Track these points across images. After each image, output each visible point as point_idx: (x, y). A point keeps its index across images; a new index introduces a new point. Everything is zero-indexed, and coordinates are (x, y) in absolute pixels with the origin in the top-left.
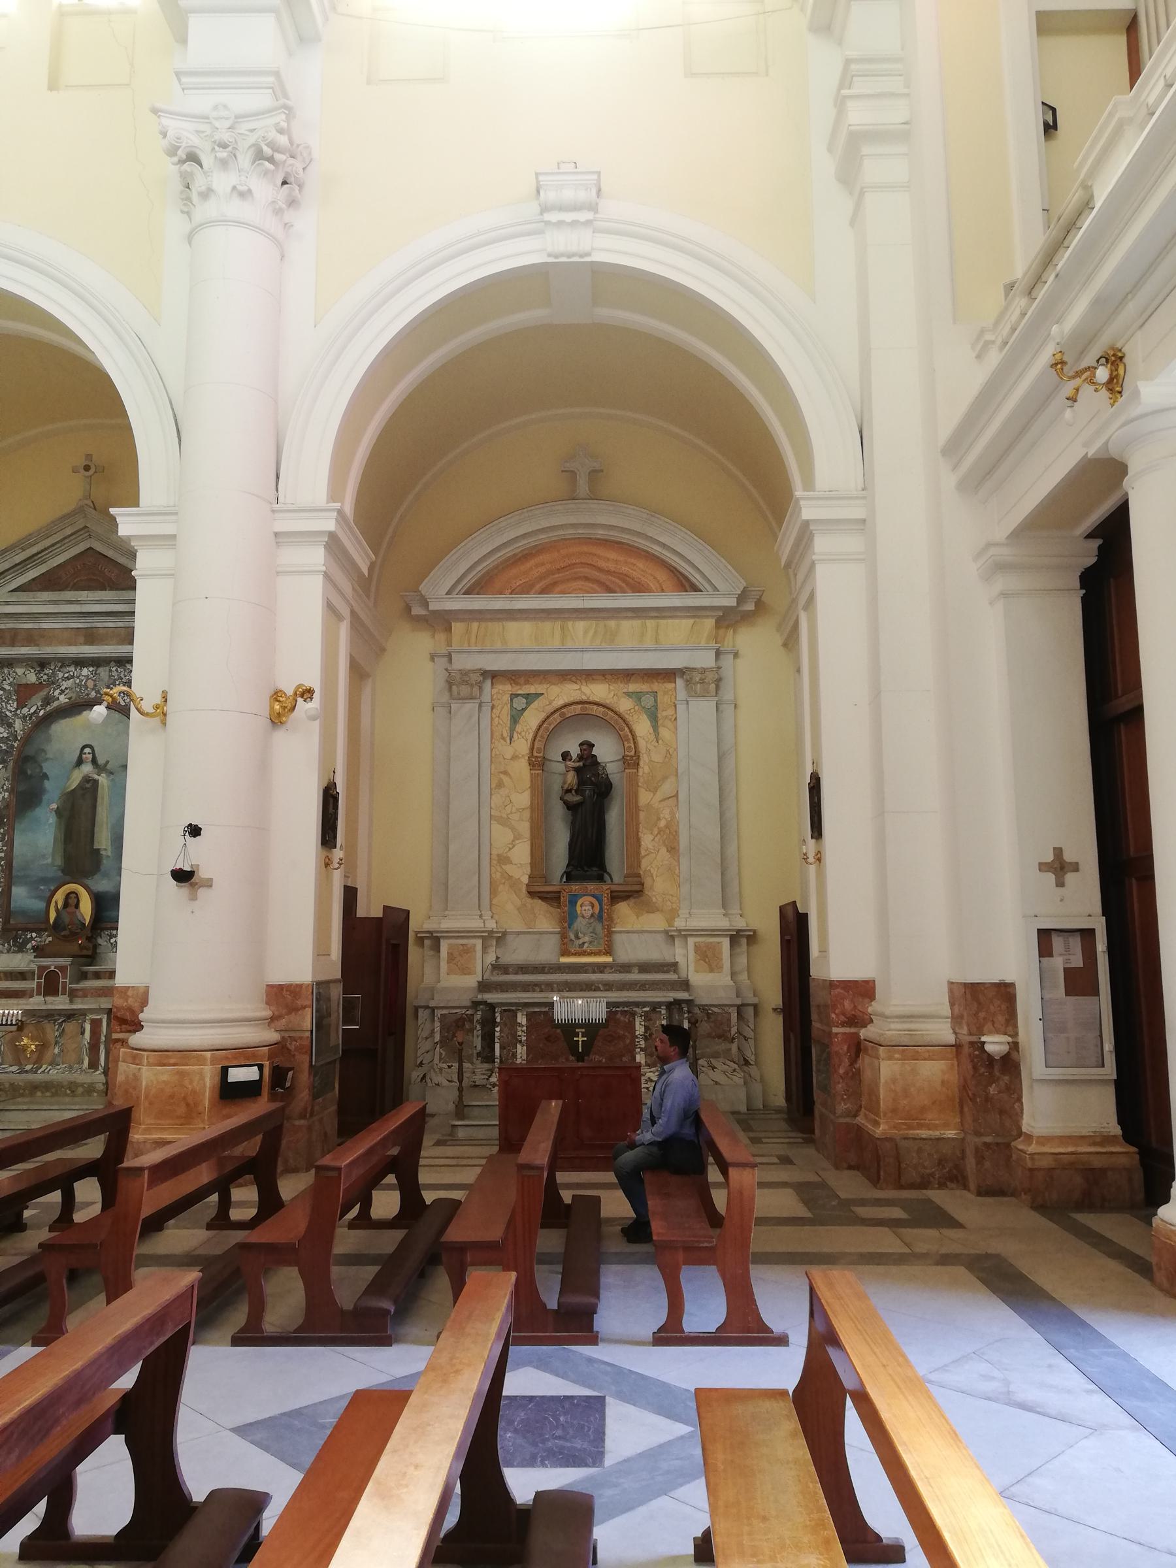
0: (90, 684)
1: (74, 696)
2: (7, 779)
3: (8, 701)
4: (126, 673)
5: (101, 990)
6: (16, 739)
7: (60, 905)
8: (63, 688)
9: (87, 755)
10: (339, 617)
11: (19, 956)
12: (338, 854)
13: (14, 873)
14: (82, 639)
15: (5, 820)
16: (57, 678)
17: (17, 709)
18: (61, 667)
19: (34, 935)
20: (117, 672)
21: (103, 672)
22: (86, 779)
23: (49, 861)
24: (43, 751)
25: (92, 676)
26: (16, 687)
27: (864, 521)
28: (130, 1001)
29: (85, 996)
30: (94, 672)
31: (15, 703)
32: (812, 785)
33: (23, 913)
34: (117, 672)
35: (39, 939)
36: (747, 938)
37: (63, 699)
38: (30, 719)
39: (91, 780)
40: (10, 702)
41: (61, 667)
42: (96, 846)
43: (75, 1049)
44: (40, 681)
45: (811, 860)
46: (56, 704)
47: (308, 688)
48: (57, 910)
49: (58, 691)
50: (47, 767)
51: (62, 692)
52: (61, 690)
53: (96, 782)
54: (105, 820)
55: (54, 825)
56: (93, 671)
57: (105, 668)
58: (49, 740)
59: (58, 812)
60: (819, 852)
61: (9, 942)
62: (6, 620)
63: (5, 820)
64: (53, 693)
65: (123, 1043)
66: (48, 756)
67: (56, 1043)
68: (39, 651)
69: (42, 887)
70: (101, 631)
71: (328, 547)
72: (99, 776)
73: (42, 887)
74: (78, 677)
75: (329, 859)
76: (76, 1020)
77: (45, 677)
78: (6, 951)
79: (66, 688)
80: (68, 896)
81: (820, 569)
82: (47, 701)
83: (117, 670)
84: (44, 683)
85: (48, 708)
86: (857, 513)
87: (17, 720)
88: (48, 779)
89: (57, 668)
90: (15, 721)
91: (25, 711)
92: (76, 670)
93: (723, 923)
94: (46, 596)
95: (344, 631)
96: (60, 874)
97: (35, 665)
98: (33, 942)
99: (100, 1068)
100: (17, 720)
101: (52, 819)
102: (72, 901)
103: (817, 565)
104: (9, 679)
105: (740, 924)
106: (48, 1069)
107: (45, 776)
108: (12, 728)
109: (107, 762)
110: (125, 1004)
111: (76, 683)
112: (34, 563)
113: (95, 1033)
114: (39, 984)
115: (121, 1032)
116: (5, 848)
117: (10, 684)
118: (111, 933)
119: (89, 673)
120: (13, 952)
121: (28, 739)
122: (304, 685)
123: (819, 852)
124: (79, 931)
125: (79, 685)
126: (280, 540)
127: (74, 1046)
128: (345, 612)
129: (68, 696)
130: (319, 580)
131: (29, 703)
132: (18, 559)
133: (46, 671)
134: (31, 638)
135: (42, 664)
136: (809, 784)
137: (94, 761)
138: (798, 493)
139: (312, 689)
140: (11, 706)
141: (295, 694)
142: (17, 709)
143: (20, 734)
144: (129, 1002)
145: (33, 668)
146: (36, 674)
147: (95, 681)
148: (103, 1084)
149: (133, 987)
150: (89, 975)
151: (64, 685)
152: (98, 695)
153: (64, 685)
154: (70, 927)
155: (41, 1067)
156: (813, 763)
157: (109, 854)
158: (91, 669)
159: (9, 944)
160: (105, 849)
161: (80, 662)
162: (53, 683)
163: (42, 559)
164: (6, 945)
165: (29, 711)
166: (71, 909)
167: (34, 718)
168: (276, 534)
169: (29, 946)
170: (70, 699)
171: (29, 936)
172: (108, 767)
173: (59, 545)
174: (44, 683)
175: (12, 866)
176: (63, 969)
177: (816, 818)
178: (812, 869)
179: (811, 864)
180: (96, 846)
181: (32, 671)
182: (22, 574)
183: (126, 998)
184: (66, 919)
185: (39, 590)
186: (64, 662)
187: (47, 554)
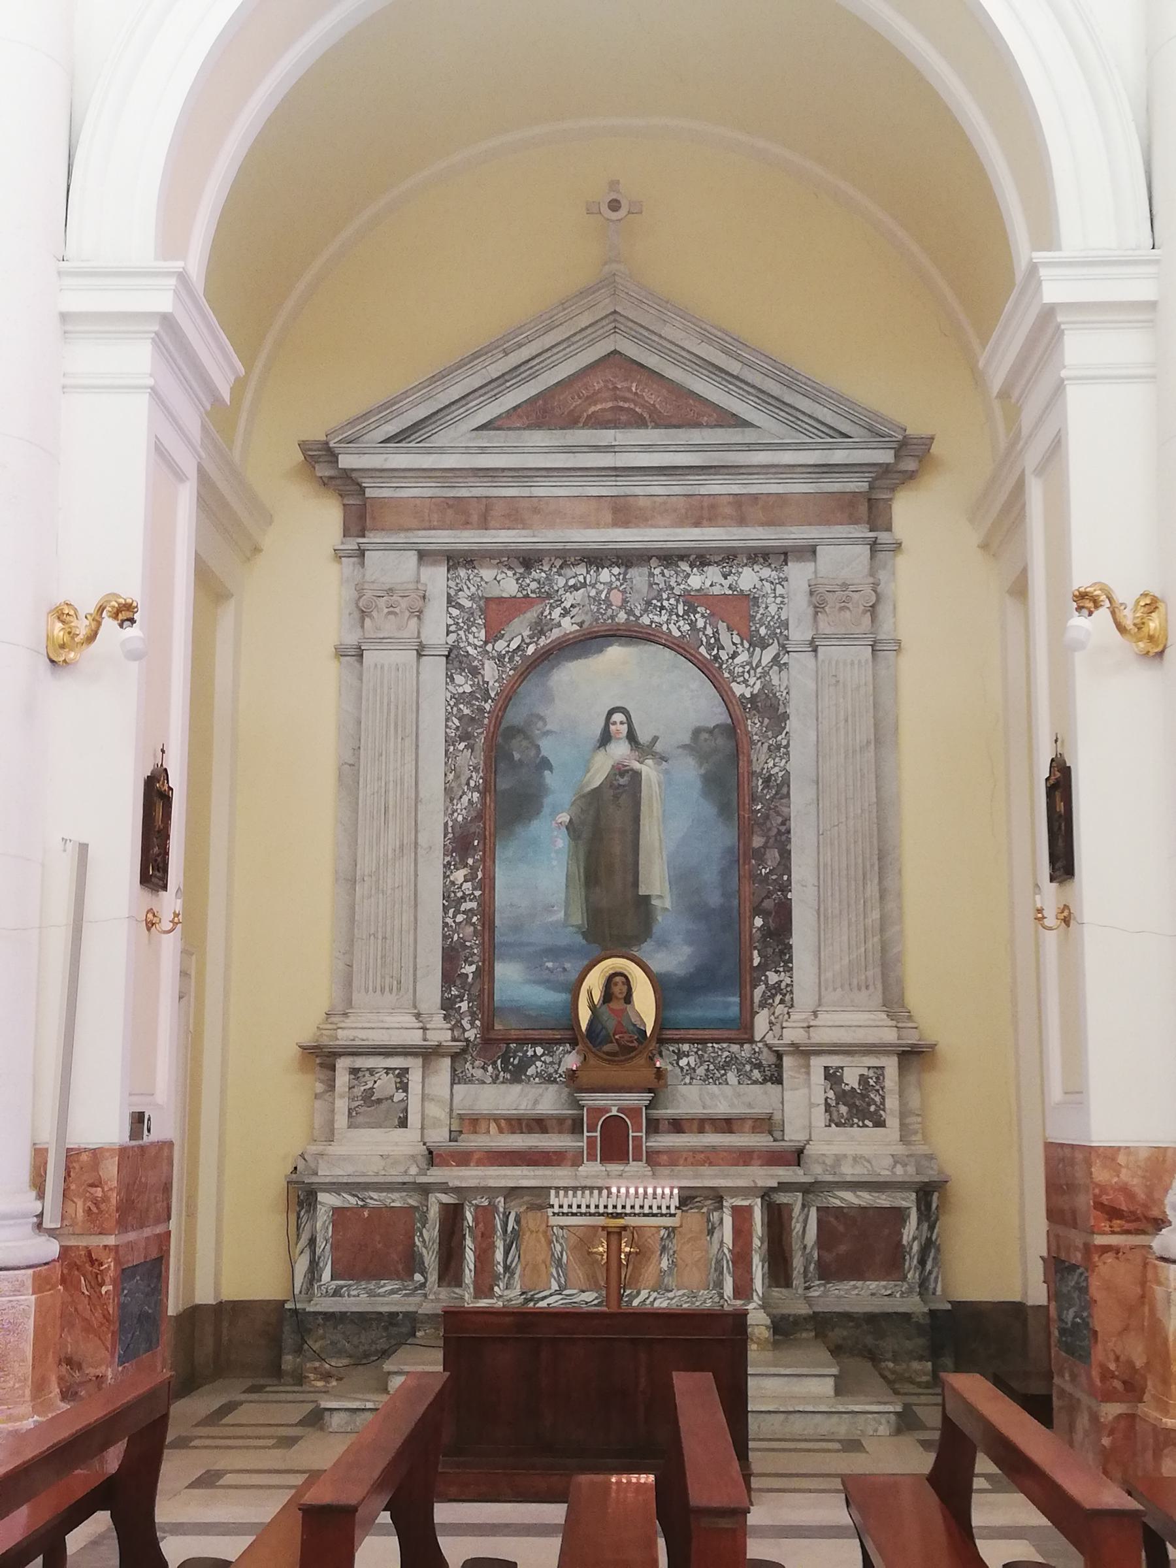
0: (616, 598)
1: (588, 619)
2: (476, 769)
3: (469, 627)
4: (679, 580)
5: (702, 1152)
6: (486, 697)
7: (597, 997)
8: (567, 605)
9: (619, 727)
10: (180, 477)
11: (516, 1089)
12: (169, 902)
13: (498, 938)
14: (608, 517)
15: (476, 843)
16: (556, 588)
17: (486, 643)
18: (561, 567)
19: (539, 1051)
20: (663, 575)
21: (638, 576)
22: (619, 769)
23: (561, 915)
24: (541, 718)
25: (619, 584)
26: (482, 603)
27: (1152, 305)
28: (1125, 1175)
29: (673, 1163)
30: (621, 577)
31: (483, 631)
32: (1052, 782)
33: (517, 1010)
34: (663, 575)
35: (548, 1059)
36: (452, 1056)
37: (568, 626)
38: (511, 660)
39: (627, 771)
40: (474, 629)
41: (561, 567)
42: (642, 891)
43: (699, 1261)
44: (525, 592)
45: (1050, 921)
46: (555, 634)
47: (129, 601)
48: (593, 1007)
49: (558, 611)
50: (547, 747)
51: (566, 612)
52: (564, 609)
53: (637, 775)
54: (657, 844)
55: (566, 850)
56: (620, 574)
57: (641, 569)
58: (548, 698)
59: (572, 828)
60: (1066, 907)
61: (494, 1063)
62: (471, 481)
63: (476, 843)
64: (550, 614)
65: (1117, 1253)
66: (548, 727)
67: (664, 1249)
68: (534, 536)
69: (550, 965)
70: (642, 502)
71: (158, 341)
72: (641, 763)
73: (550, 965)
74: (593, 586)
75: (154, 915)
76: (697, 1207)
77: (534, 585)
78: (489, 1080)
79: (572, 606)
80: (610, 981)
81: (1073, 393)
82: (540, 629)
83: (663, 574)
84: (533, 595)
85: (543, 641)
86: (1140, 289)
87: (487, 662)
88: (551, 768)
89: (555, 570)
90: (483, 665)
91: (501, 645)
92: (588, 572)
93: (889, 1036)
94: (539, 438)
95: (186, 498)
96: (580, 939)
97: (514, 563)
98: (538, 1064)
99: (755, 1297)
100: (487, 662)
101: (562, 841)
102: (619, 990)
103: (1068, 388)
104: (469, 588)
105: (911, 1038)
106: (651, 1299)
107: (545, 764)
108: (480, 677)
109: (655, 739)
110: (1116, 1179)
111: (589, 596)
112: (519, 378)
113: (742, 1231)
114: (591, 1142)
115: (1113, 1233)
116: (477, 893)
117: (472, 598)
118: (679, 1050)
119: (614, 579)
120: (503, 1082)
121: (508, 697)
122: (119, 596)
123: (1065, 906)
124: (635, 1044)
125: (596, 600)
126: (69, 328)
127: (697, 1255)
128: (189, 466)
129: (578, 619)
130: (141, 403)
131: (508, 632)
132: (494, 371)
133: (535, 574)
134: (515, 515)
135: (527, 560)
136: (1047, 779)
137: (631, 737)
138: (1024, 252)
139: (135, 604)
140: (474, 637)
141: (101, 609)
142: (486, 643)
143: (494, 688)
144: (1122, 1176)
145: (510, 568)
146: (517, 580)
147: (624, 592)
148: (767, 1327)
149: (1128, 1147)
150: (664, 1125)
151: (569, 599)
152: (632, 618)
153: (569, 599)
154: (617, 1037)
155: (638, 1293)
156: (1056, 741)
157: (668, 905)
158: (616, 570)
159: (495, 1068)
160: (660, 897)
161: (595, 559)
162: (549, 596)
163: (533, 370)
164: (490, 1068)
165: (508, 646)
166: (614, 1005)
167: (517, 658)
168: (64, 317)
169: (531, 1071)
170: (581, 624)
171: (530, 1053)
172: (658, 747)
173: (565, 345)
174: (533, 595)
175: (494, 927)
176: (634, 1112)
177: (1061, 843)
178: (1051, 939)
179: (1050, 929)
180: (642, 891)
181: (510, 573)
182: (495, 397)
183: (1117, 1169)
184: (610, 1023)
185: (529, 427)
186: (567, 558)
187: (538, 364)
